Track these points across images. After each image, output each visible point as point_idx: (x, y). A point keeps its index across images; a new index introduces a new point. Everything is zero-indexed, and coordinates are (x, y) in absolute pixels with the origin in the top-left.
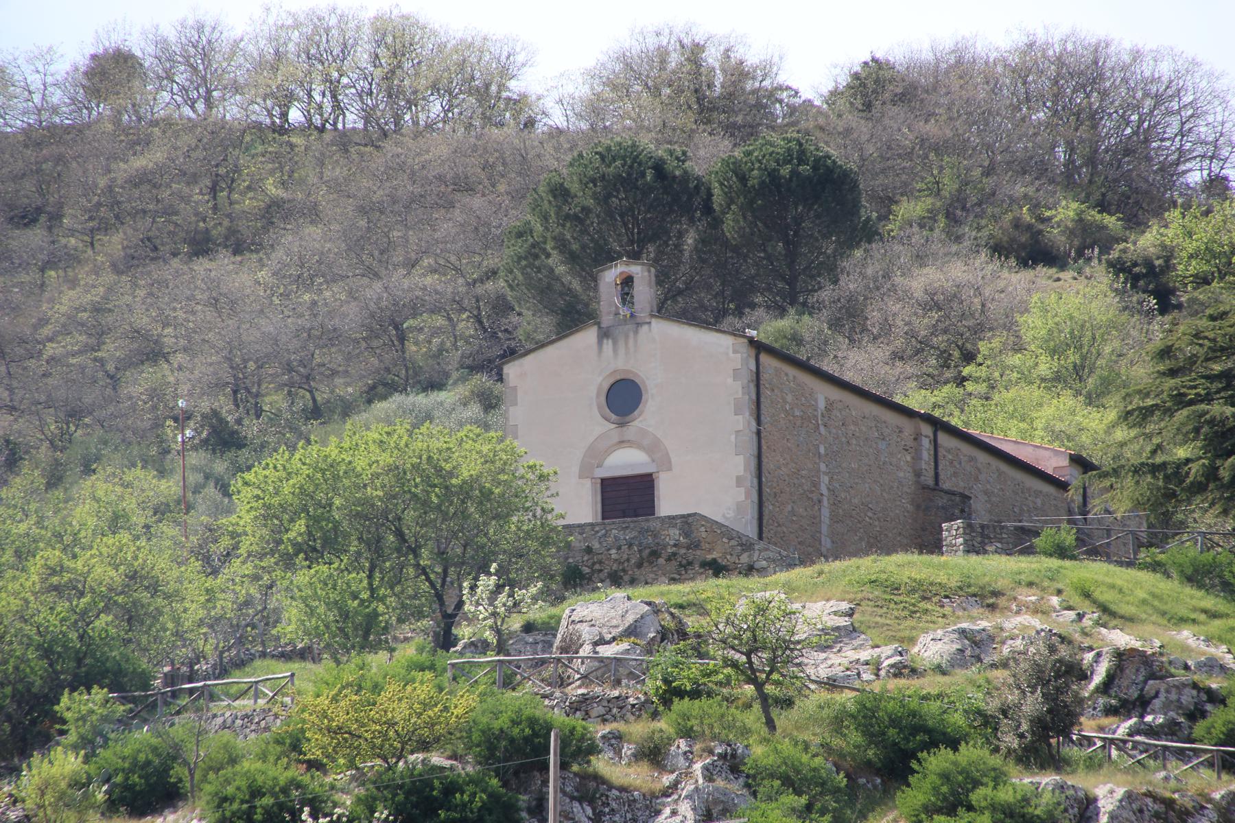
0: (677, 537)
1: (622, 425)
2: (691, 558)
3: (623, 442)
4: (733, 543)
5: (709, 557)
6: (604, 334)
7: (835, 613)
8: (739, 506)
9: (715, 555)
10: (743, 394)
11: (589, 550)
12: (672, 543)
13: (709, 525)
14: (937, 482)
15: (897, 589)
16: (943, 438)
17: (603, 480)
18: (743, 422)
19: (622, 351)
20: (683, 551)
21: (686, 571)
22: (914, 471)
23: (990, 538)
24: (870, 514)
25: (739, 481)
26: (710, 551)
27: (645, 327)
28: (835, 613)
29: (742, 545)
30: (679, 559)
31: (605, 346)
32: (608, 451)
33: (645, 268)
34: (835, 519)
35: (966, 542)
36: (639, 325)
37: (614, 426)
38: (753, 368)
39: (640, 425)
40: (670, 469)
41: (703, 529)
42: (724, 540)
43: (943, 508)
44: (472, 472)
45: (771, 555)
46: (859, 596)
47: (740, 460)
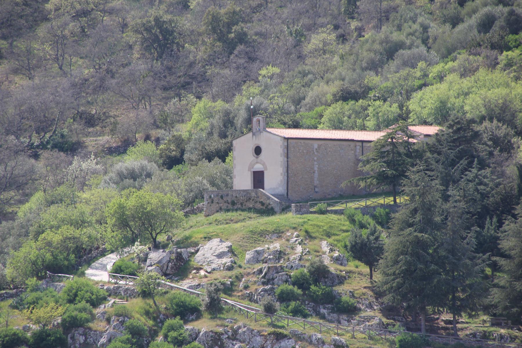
1: (257, 158)
6: (254, 134)
11: (236, 197)
17: (254, 172)
25: (281, 174)
32: (254, 165)
36: (261, 132)
47: (281, 169)
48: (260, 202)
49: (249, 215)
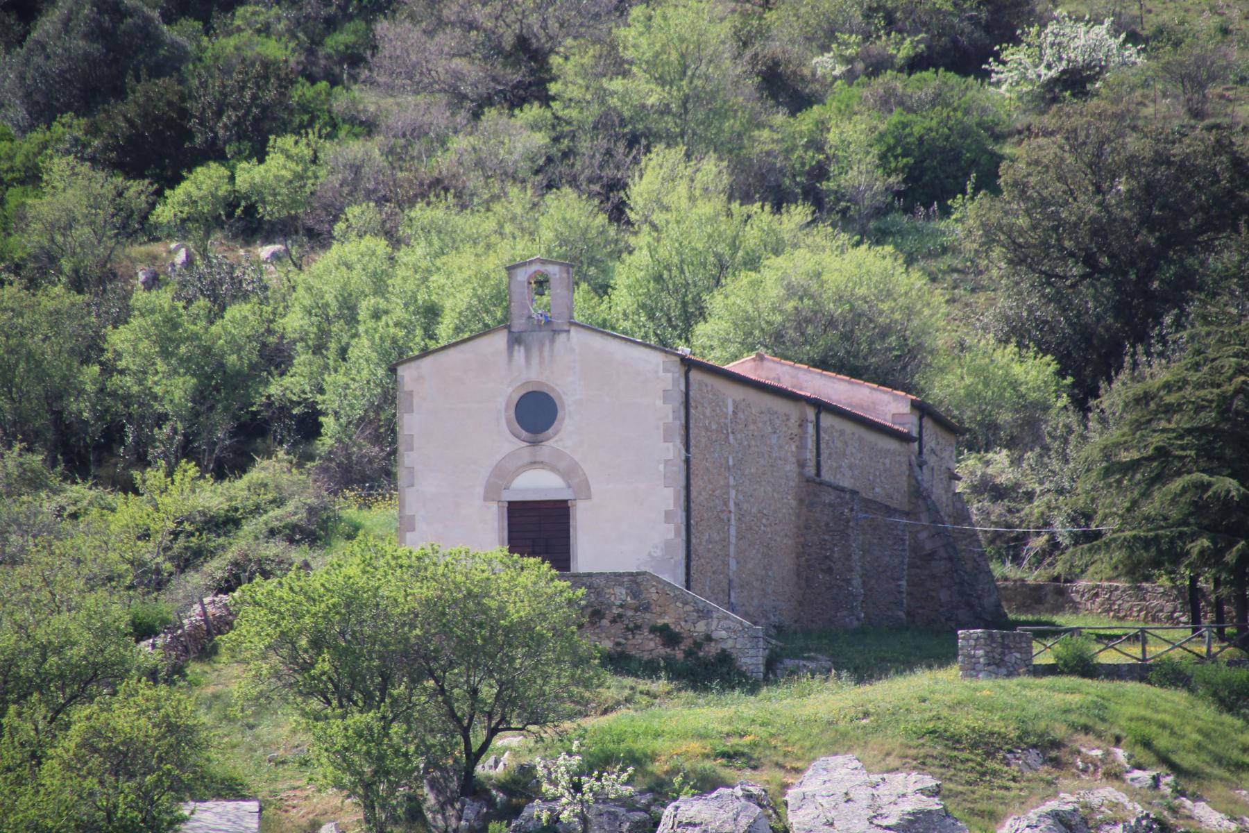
0: (623, 597)
1: (534, 443)
2: (639, 622)
3: (535, 463)
4: (688, 608)
5: (660, 622)
6: (516, 340)
7: (922, 791)
8: (668, 545)
9: (666, 620)
10: (674, 418)
12: (618, 603)
13: (660, 586)
14: (818, 474)
15: (958, 742)
16: (827, 420)
18: (673, 450)
19: (535, 360)
20: (630, 613)
21: (633, 634)
22: (798, 461)
23: (1010, 648)
24: (764, 521)
25: (668, 516)
26: (661, 615)
27: (563, 336)
28: (922, 791)
29: (698, 611)
30: (626, 622)
31: (516, 354)
32: (517, 472)
33: (564, 268)
34: (741, 537)
35: (987, 653)
36: (556, 332)
37: (525, 444)
38: (683, 387)
39: (555, 445)
40: (589, 497)
41: (653, 590)
42: (678, 604)
43: (830, 505)
44: (522, 614)
45: (731, 624)
46: (922, 752)
48: (654, 630)
49: (643, 685)
